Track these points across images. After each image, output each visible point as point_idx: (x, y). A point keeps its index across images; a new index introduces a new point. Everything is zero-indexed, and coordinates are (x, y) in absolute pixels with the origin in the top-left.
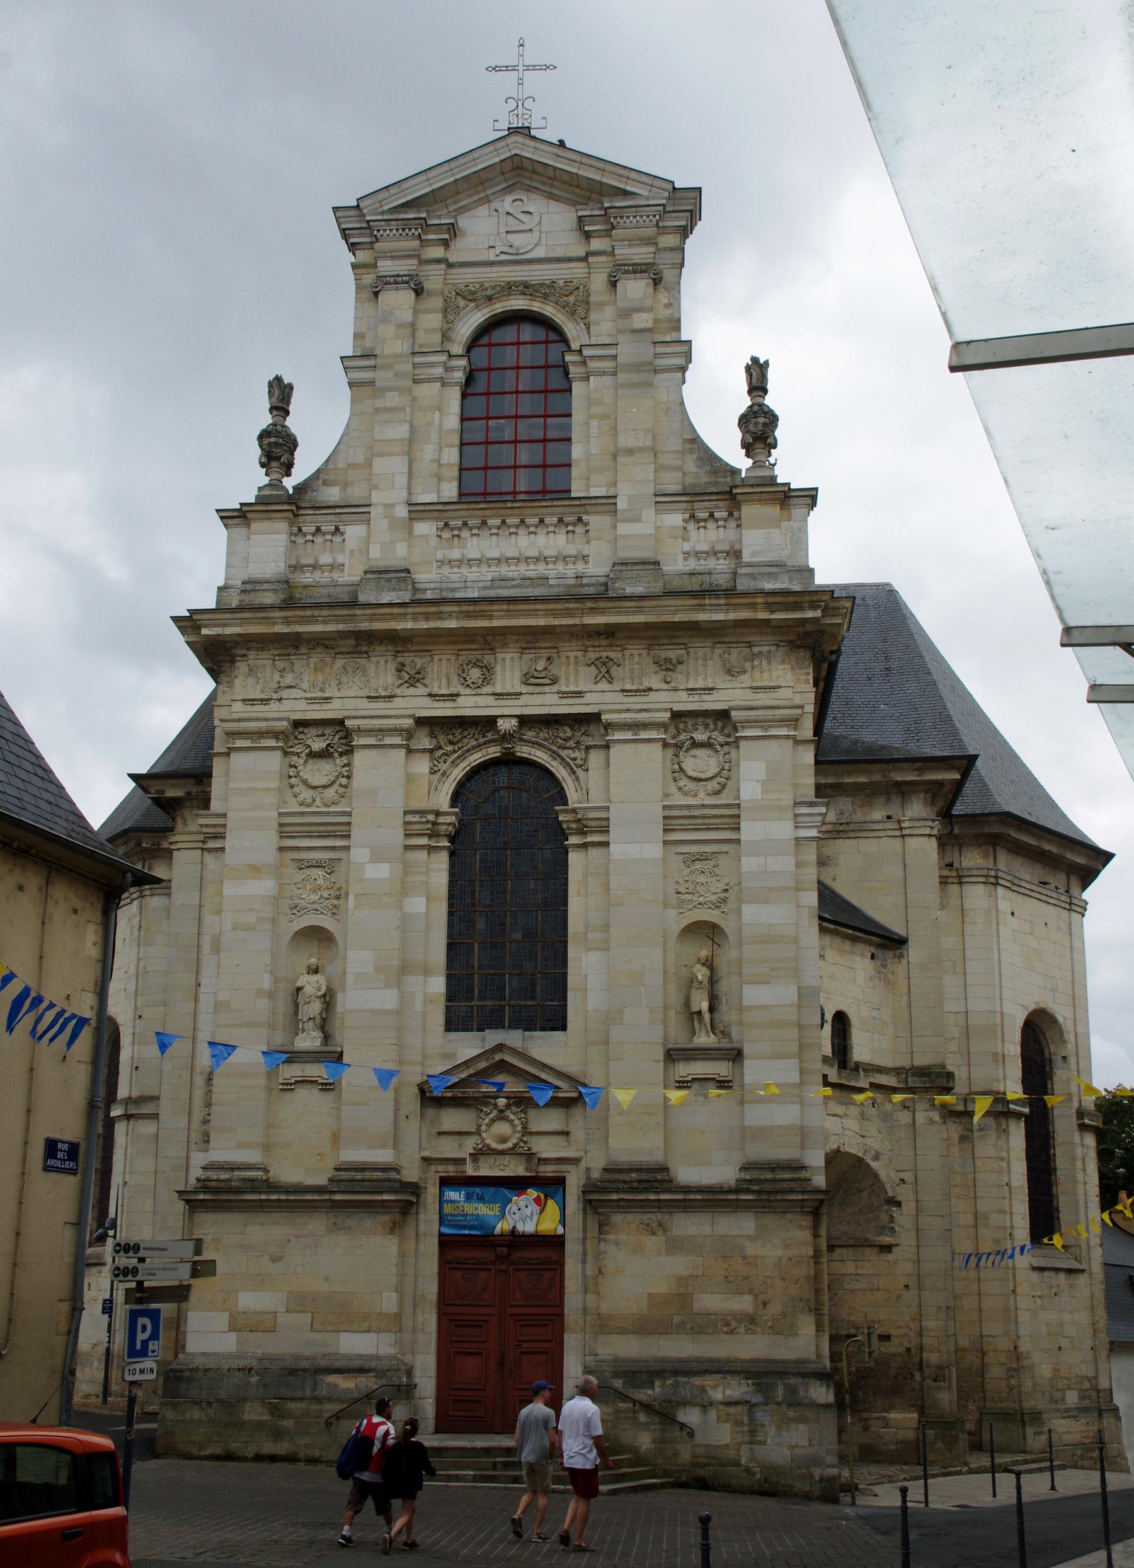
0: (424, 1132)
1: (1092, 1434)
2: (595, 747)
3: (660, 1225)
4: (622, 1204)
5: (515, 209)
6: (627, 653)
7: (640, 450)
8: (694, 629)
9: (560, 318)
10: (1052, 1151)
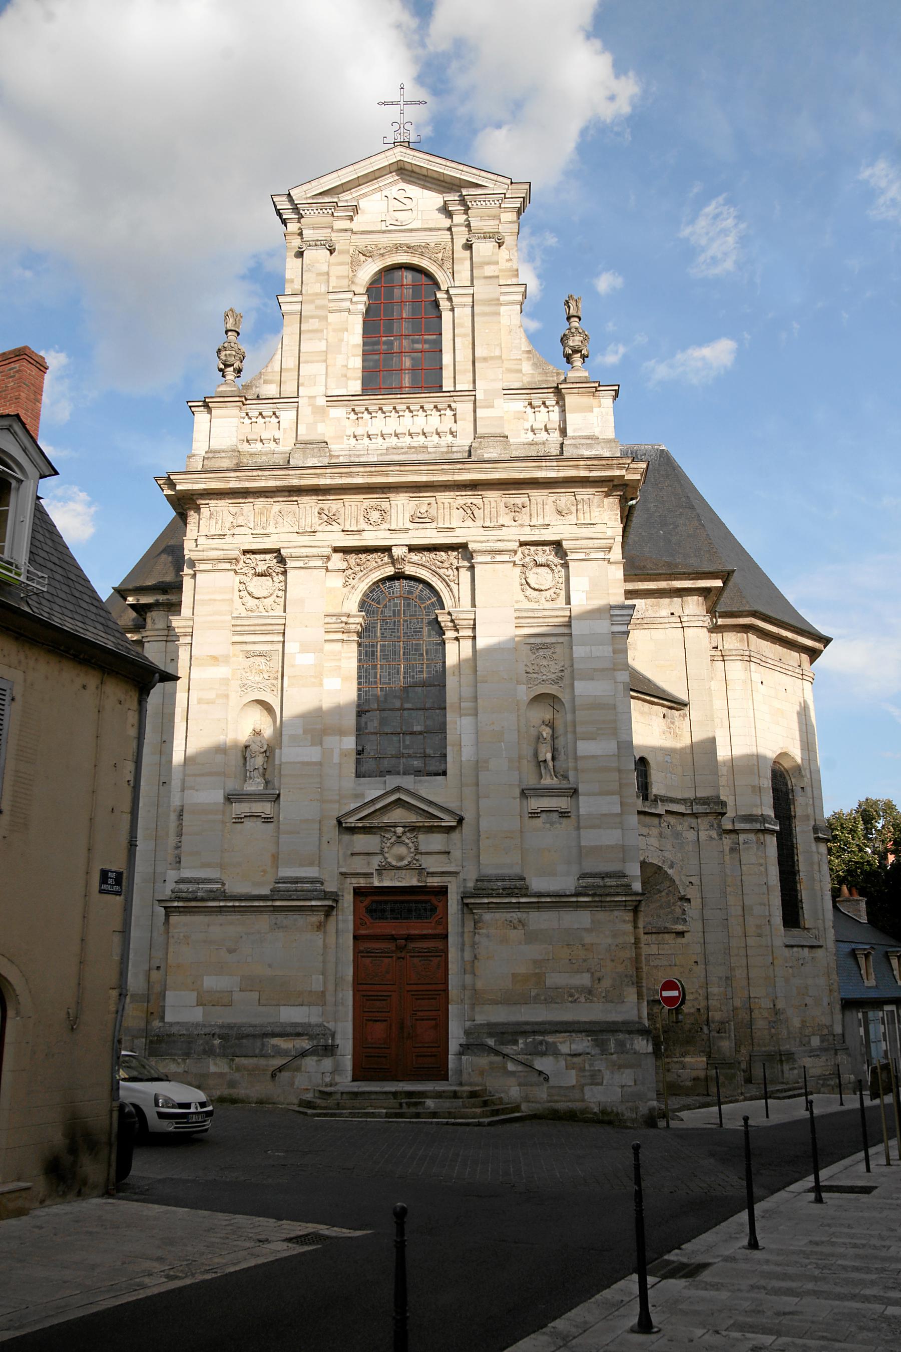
4: (490, 906)
9: (432, 268)
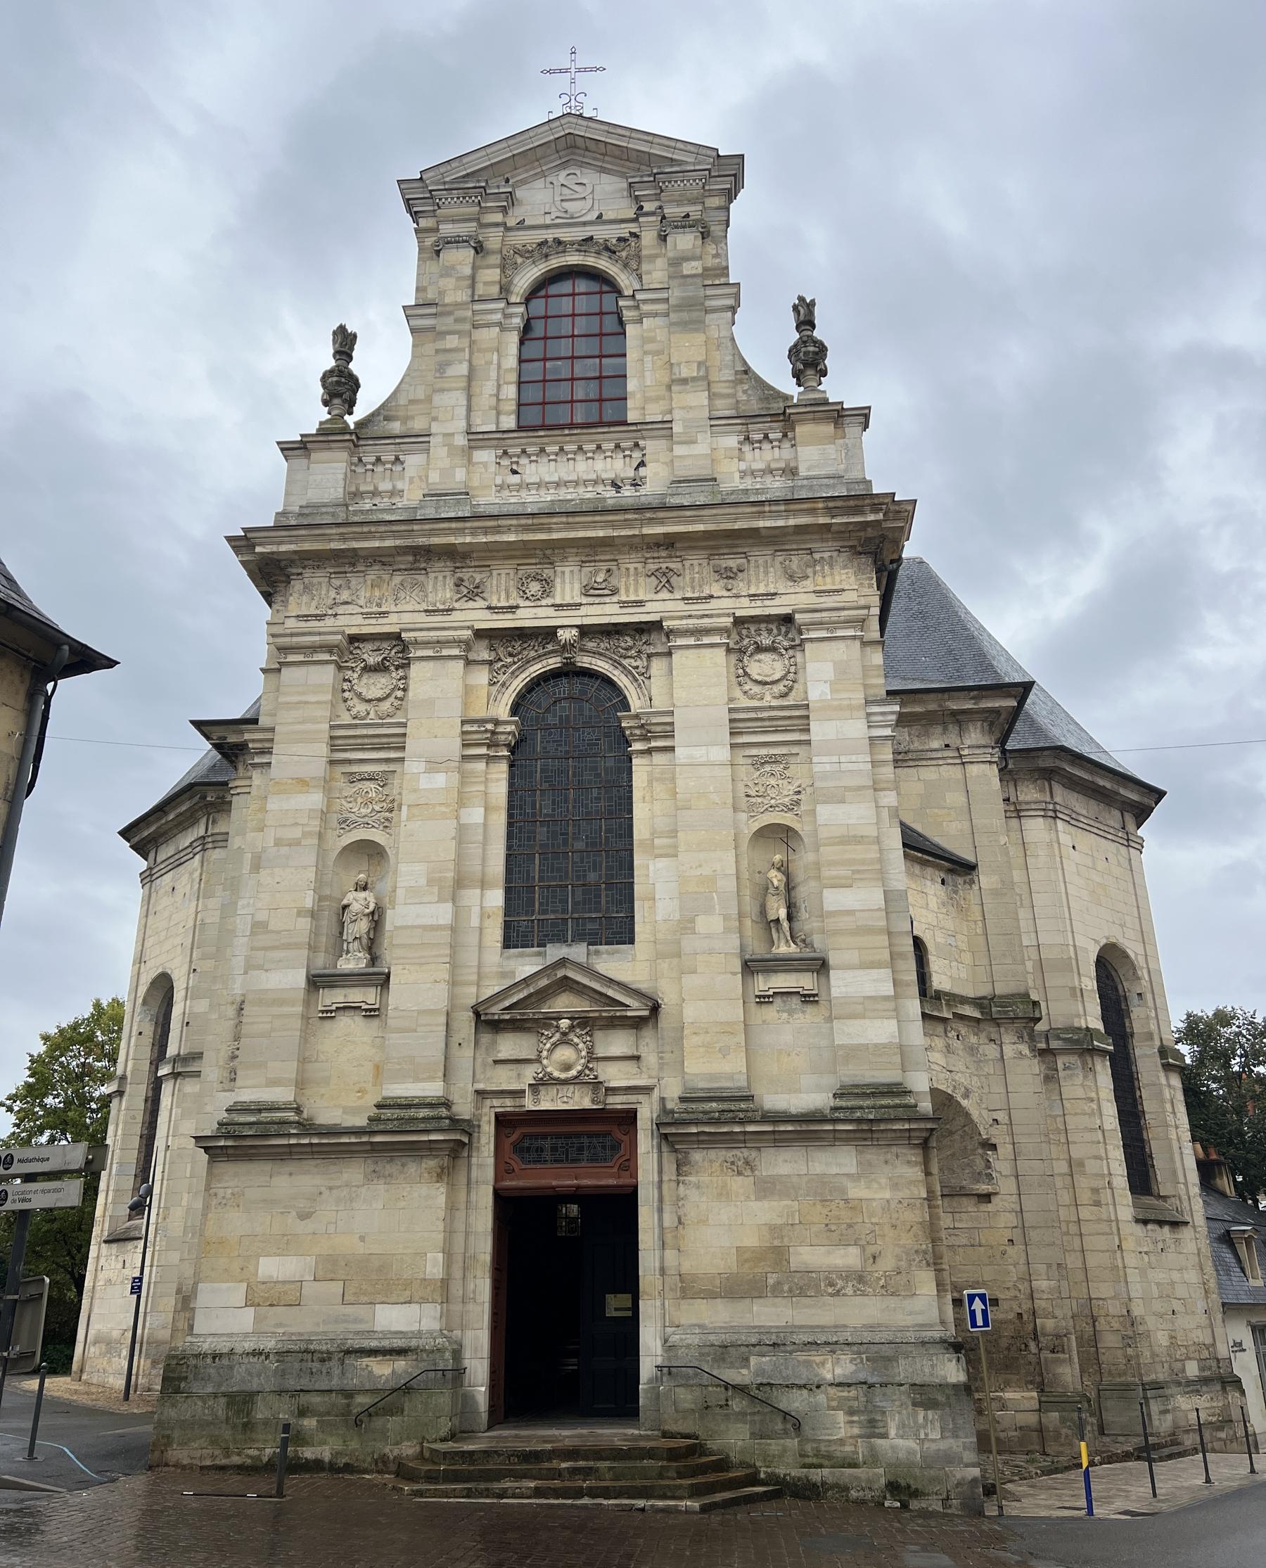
0: (479, 1061)
1: (1217, 1411)
2: (657, 654)
3: (747, 1163)
4: (702, 1138)
5: (570, 182)
6: (687, 563)
7: (694, 379)
8: (754, 535)
10: (1138, 1094)
